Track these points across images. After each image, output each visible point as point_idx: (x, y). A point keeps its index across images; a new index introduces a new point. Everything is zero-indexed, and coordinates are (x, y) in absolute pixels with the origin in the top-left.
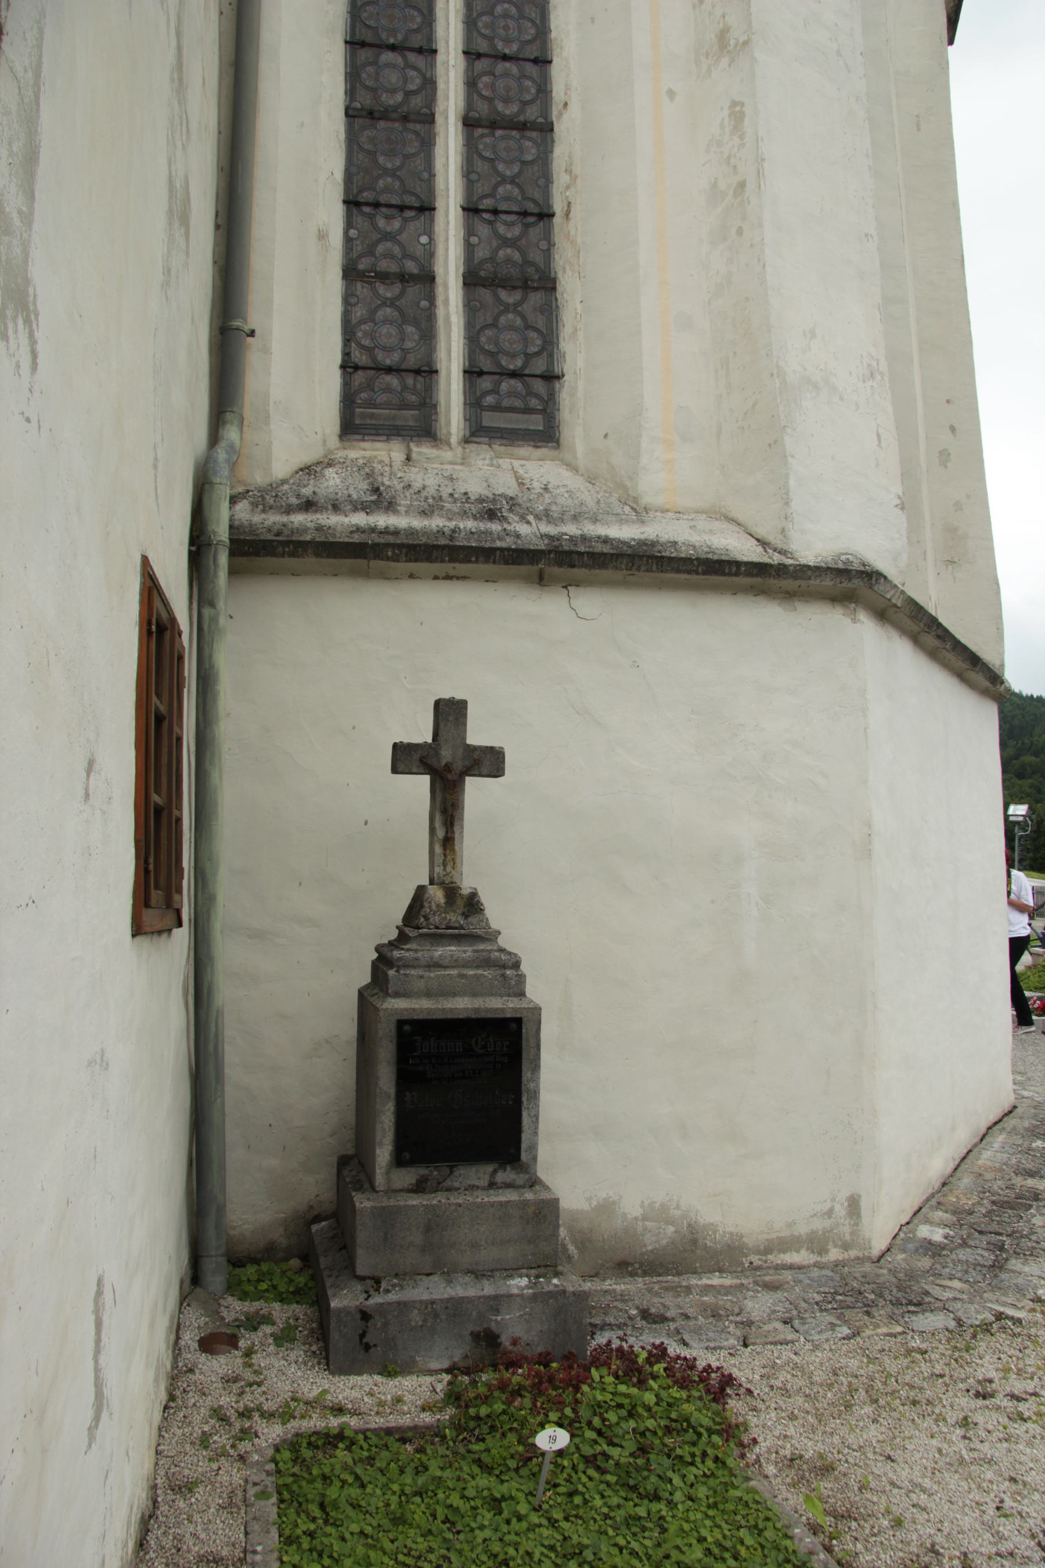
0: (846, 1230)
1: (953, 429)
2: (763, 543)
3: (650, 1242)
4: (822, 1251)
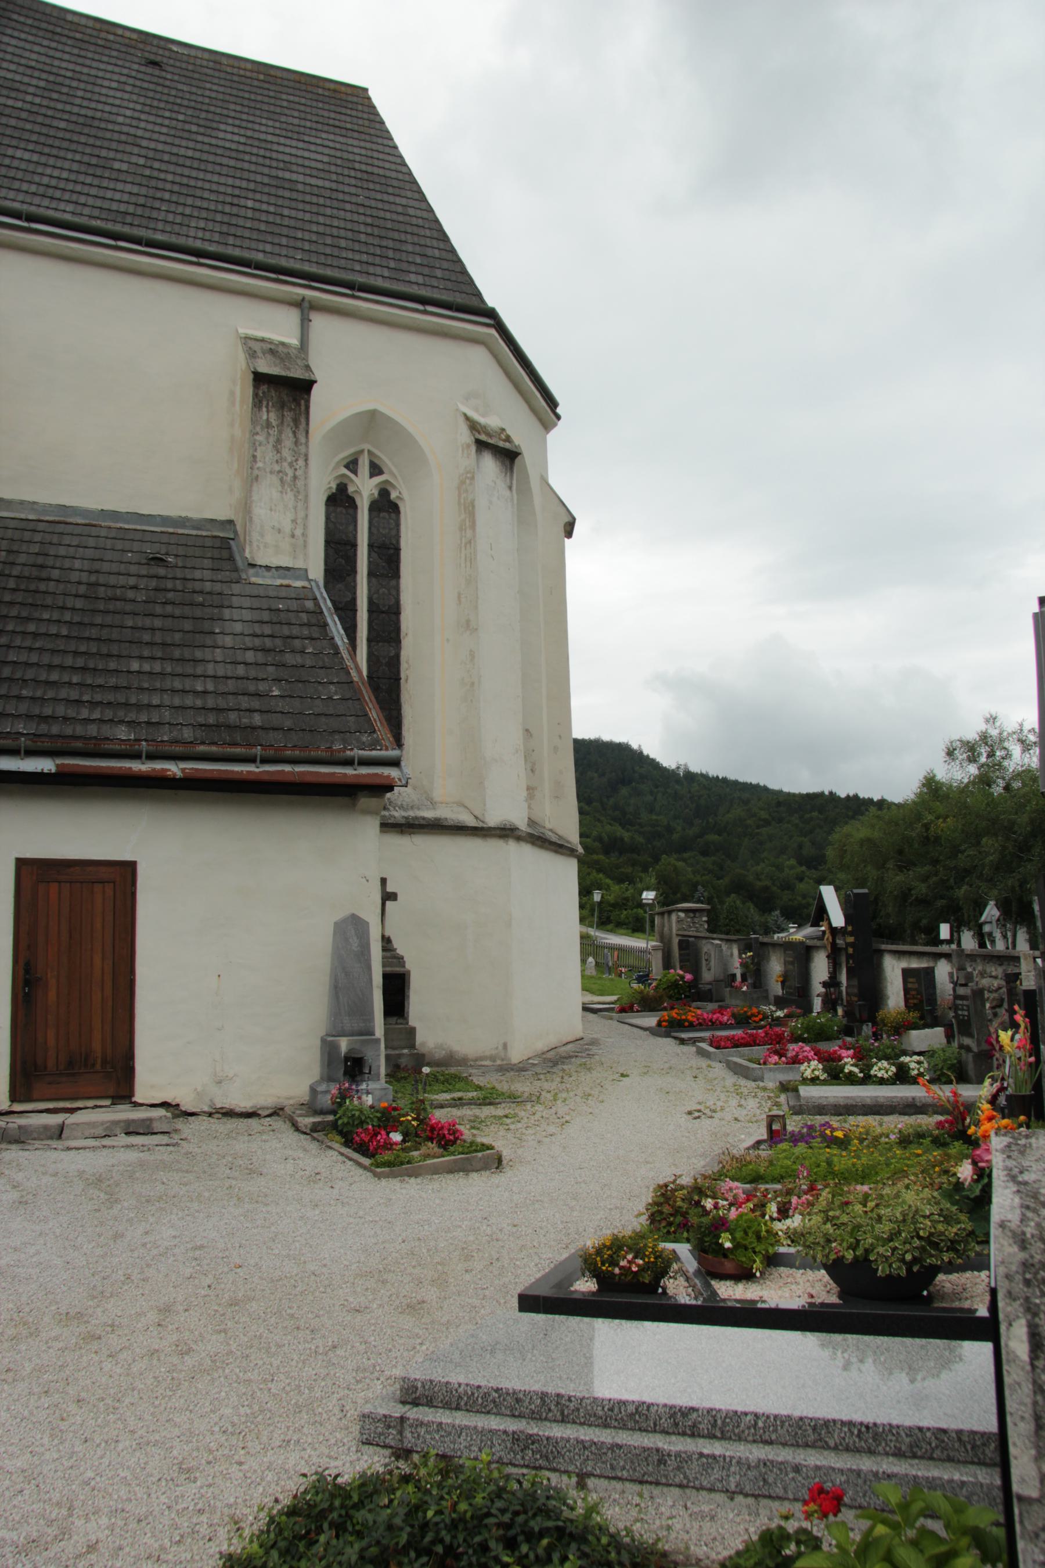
0: (502, 1054)
1: (560, 737)
2: (476, 818)
3: (437, 1056)
4: (494, 1061)
